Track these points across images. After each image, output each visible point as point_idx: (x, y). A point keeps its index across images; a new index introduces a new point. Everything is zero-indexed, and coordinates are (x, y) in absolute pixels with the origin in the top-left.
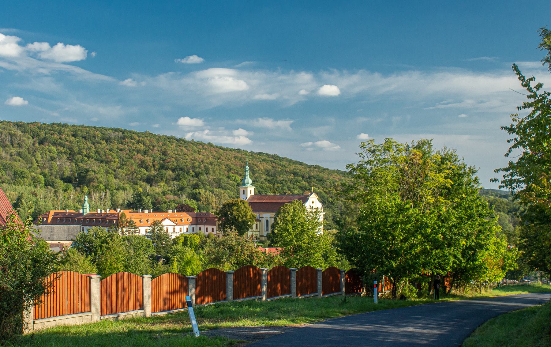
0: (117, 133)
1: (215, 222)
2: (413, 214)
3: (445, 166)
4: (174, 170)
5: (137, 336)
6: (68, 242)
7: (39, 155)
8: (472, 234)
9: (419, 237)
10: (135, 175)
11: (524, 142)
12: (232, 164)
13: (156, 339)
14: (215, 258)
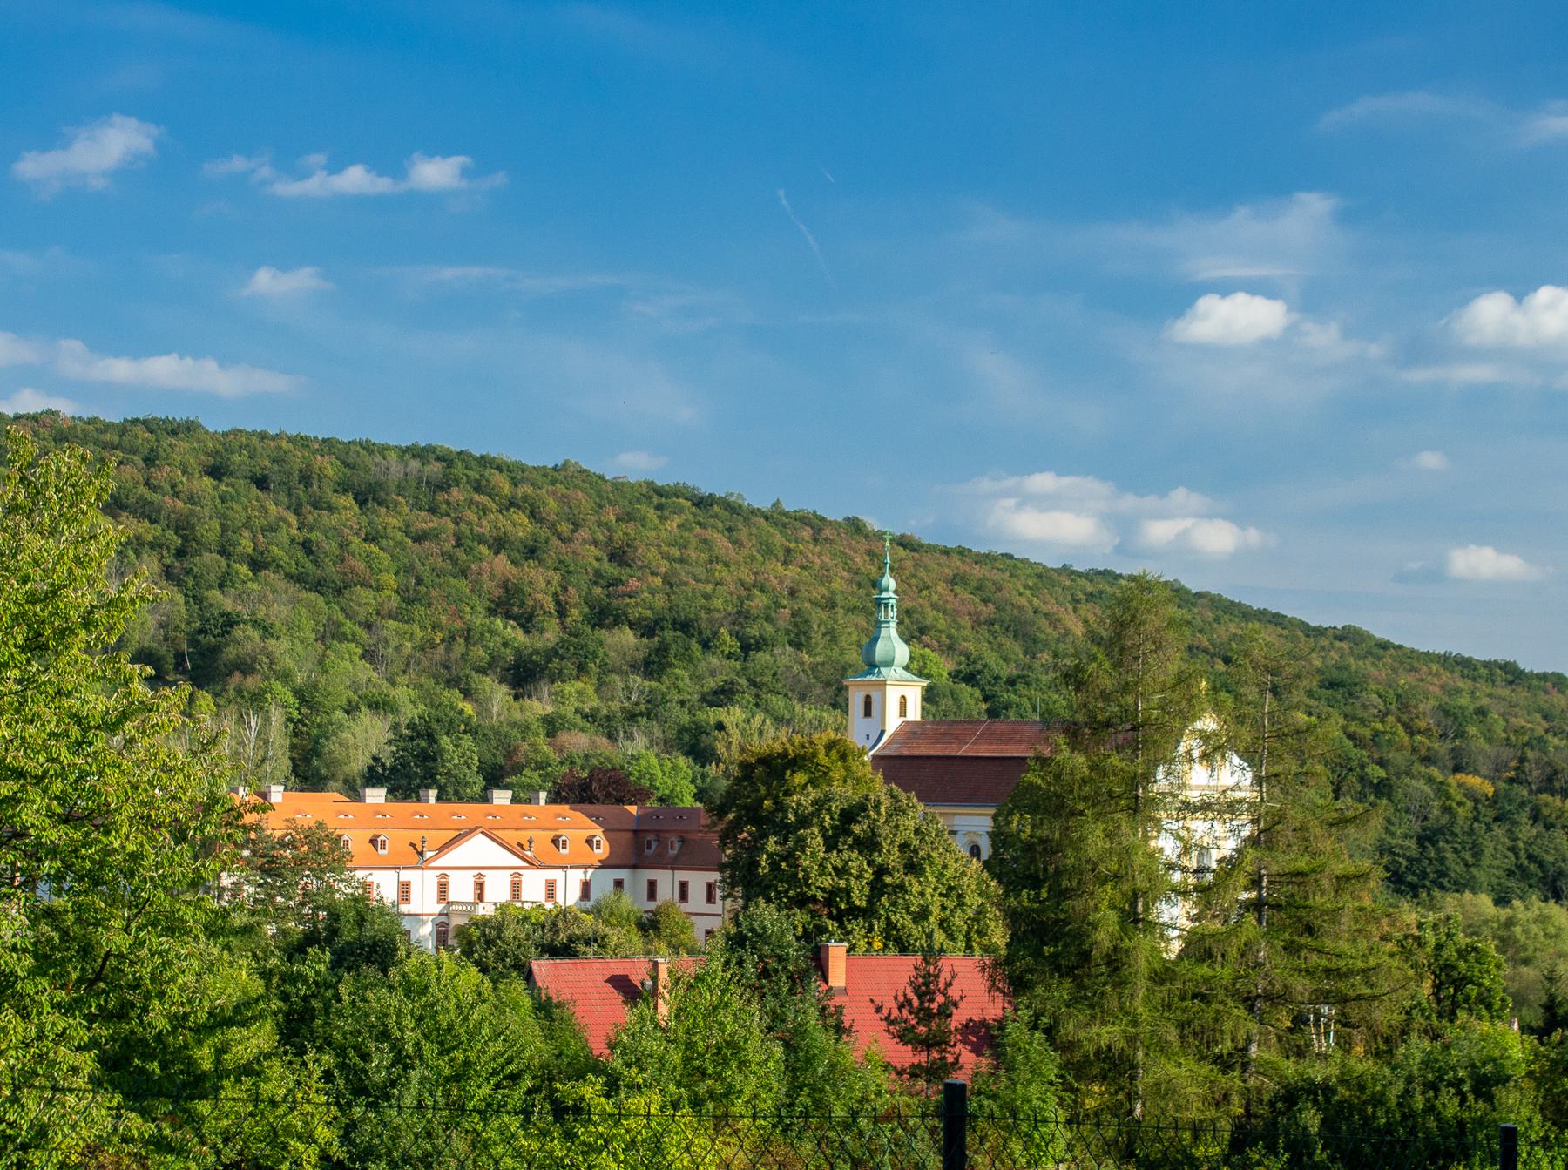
4: (647, 629)
10: (459, 647)
12: (934, 606)
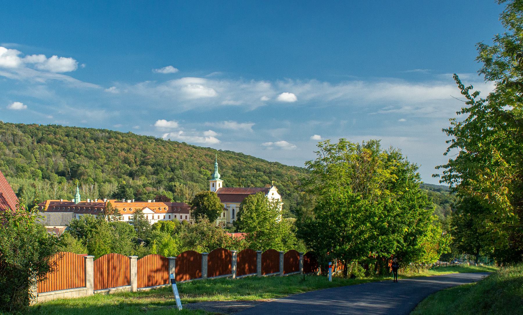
0: (104, 134)
1: (188, 210)
2: (362, 205)
3: (390, 163)
4: (153, 166)
5: (128, 308)
6: (62, 227)
7: (37, 152)
8: (413, 222)
9: (368, 224)
10: (119, 170)
11: (460, 143)
12: (203, 160)
13: (145, 311)
14: (189, 242)
